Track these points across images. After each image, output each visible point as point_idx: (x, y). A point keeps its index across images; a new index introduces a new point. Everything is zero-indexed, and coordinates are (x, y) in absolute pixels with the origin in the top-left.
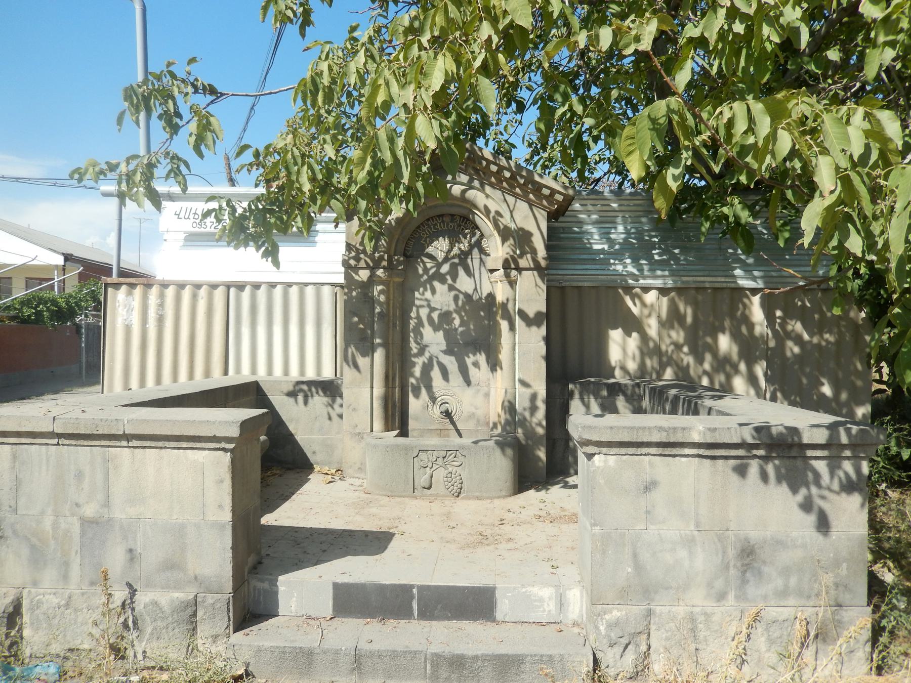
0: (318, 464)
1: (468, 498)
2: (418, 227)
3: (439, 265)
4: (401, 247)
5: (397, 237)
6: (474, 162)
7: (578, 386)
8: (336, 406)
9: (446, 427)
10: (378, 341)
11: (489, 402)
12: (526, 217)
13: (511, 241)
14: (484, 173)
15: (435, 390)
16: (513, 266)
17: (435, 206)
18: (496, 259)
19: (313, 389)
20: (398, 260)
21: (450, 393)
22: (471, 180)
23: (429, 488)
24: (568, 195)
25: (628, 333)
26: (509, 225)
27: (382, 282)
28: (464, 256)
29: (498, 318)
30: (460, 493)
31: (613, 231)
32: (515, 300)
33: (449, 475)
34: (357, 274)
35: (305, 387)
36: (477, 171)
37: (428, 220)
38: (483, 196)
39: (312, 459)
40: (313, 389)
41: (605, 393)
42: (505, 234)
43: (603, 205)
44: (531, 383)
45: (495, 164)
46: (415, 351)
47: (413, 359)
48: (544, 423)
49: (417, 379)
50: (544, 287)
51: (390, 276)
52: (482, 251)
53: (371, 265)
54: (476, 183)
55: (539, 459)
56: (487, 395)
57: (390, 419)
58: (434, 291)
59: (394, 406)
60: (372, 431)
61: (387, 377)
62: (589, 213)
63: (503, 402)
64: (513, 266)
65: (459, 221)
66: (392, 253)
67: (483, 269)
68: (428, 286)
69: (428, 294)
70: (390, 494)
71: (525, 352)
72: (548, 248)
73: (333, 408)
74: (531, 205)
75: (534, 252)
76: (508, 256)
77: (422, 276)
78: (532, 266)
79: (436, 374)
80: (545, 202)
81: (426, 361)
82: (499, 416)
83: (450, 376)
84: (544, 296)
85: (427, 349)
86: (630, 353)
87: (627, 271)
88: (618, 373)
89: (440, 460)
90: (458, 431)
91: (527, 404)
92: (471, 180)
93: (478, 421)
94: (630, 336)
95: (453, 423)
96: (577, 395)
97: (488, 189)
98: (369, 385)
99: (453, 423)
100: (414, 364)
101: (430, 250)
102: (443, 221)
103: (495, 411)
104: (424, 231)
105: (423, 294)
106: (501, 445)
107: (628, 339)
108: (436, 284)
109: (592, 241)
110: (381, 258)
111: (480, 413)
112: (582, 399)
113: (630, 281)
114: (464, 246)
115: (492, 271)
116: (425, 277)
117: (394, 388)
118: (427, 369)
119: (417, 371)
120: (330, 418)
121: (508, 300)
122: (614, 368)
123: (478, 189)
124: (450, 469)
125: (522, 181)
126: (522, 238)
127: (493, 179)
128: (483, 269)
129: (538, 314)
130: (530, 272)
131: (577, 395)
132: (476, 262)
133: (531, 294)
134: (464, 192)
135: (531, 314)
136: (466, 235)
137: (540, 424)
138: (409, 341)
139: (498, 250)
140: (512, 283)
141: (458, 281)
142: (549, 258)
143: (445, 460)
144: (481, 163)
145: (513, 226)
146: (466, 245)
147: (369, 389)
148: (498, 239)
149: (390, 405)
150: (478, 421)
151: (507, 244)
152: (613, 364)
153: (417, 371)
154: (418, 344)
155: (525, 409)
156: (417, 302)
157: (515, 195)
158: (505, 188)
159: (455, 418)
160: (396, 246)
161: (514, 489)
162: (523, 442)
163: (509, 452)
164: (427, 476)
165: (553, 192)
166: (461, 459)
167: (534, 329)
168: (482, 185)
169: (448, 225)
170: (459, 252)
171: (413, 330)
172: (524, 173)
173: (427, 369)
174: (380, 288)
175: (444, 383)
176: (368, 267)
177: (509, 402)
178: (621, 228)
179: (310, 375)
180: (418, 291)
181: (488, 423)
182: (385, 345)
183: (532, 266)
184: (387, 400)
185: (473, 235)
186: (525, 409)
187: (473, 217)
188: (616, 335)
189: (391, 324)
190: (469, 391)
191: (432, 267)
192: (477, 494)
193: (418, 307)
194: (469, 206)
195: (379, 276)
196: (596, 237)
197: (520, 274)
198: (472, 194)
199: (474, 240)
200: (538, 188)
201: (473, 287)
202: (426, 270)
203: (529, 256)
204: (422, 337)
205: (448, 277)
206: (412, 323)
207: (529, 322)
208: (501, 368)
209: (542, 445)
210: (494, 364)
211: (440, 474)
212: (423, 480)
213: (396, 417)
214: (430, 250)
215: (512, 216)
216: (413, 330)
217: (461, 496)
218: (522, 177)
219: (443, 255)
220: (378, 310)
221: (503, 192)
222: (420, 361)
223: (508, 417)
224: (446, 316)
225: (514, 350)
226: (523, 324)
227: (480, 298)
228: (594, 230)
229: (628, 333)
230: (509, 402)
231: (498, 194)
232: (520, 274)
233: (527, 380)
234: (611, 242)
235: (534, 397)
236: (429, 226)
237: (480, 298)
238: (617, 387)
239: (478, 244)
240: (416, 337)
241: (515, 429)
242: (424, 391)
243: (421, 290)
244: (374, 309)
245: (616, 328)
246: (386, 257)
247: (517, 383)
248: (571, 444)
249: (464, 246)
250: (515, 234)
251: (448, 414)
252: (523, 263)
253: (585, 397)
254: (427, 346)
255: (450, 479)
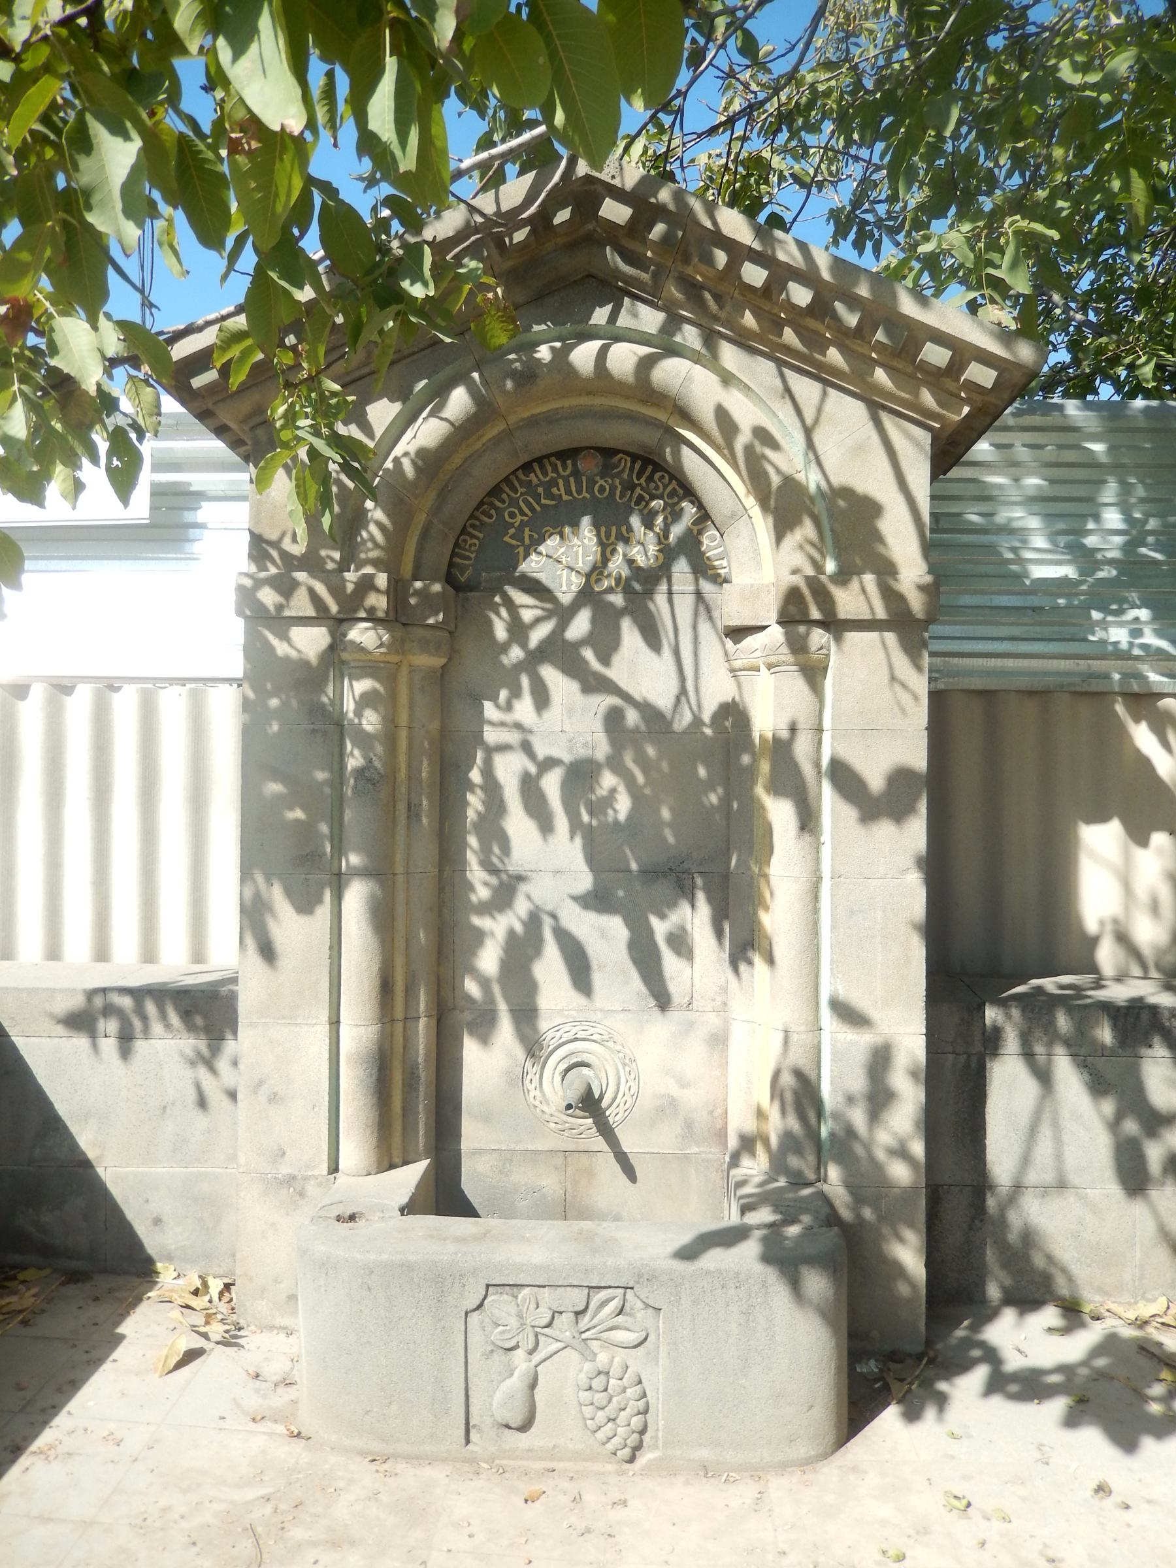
0: (169, 1258)
1: (666, 1469)
2: (495, 491)
3: (565, 615)
4: (439, 554)
5: (421, 518)
6: (686, 260)
7: (1015, 1013)
8: (222, 1064)
9: (583, 1144)
10: (354, 859)
11: (724, 1065)
12: (859, 449)
13: (807, 530)
14: (717, 298)
15: (544, 1025)
16: (815, 614)
17: (551, 419)
18: (754, 593)
19: (151, 1008)
20: (423, 594)
21: (597, 1031)
22: (673, 322)
23: (525, 1427)
24: (1018, 366)
25: (1139, 836)
26: (801, 477)
27: (368, 668)
28: (644, 583)
29: (760, 791)
30: (638, 1447)
31: (1091, 525)
32: (820, 730)
33: (598, 1383)
34: (285, 637)
35: (126, 1002)
36: (693, 290)
37: (527, 467)
38: (712, 379)
39: (151, 1240)
40: (151, 1008)
41: (1105, 1034)
42: (786, 505)
43: (1060, 447)
44: (874, 1014)
45: (758, 258)
46: (483, 893)
47: (476, 921)
48: (918, 1148)
49: (485, 983)
50: (920, 684)
51: (398, 646)
52: (703, 568)
53: (334, 608)
54: (690, 336)
55: (898, 1270)
56: (719, 1041)
57: (398, 1127)
58: (542, 699)
59: (410, 1083)
60: (334, 1169)
61: (386, 987)
62: (1012, 466)
63: (776, 1075)
64: (815, 614)
65: (627, 466)
66: (407, 569)
67: (704, 628)
68: (525, 681)
69: (524, 709)
70: (376, 1446)
71: (851, 905)
72: (928, 548)
73: (212, 1070)
74: (876, 405)
75: (886, 570)
76: (797, 580)
77: (504, 648)
78: (881, 613)
79: (550, 969)
80: (927, 398)
81: (519, 928)
82: (761, 1114)
83: (597, 978)
84: (920, 715)
85: (523, 888)
86: (1141, 891)
87: (1144, 646)
88: (1107, 956)
89: (564, 1326)
90: (622, 1159)
91: (858, 1083)
92: (673, 322)
93: (689, 1126)
94: (1143, 842)
95: (606, 1131)
96: (1011, 1042)
97: (730, 355)
98: (324, 1016)
99: (606, 1131)
100: (479, 937)
101: (532, 565)
102: (576, 473)
103: (748, 1095)
104: (514, 503)
105: (509, 707)
106: (784, 1260)
107: (1140, 854)
108: (550, 674)
109: (1028, 555)
110: (366, 585)
111: (694, 1098)
112: (1028, 1055)
113: (1153, 677)
114: (643, 549)
115: (738, 633)
116: (516, 653)
117: (410, 1019)
118: (521, 952)
119: (489, 960)
120: (202, 1102)
121: (793, 729)
122: (1094, 942)
123: (696, 359)
124: (603, 1358)
125: (852, 320)
126: (847, 525)
127: (749, 319)
128: (704, 628)
129: (900, 777)
130: (873, 636)
131: (1011, 1042)
132: (685, 605)
133: (873, 704)
134: (646, 364)
135: (876, 781)
136: (653, 514)
137: (901, 1152)
138: (464, 862)
139: (758, 562)
140: (813, 673)
141: (616, 659)
142: (931, 591)
143: (585, 1321)
144: (709, 260)
145: (812, 480)
146: (652, 549)
147: (324, 1030)
148: (762, 524)
149: (397, 1078)
150: (689, 1126)
151: (793, 539)
152: (1091, 925)
153: (489, 960)
154: (493, 870)
155: (850, 1100)
156: (491, 736)
157: (824, 376)
158: (788, 349)
159: (614, 1115)
160: (420, 549)
161: (838, 1427)
162: (846, 1214)
163: (816, 1283)
164: (516, 1383)
165: (963, 353)
166: (643, 1317)
167: (885, 829)
168: (710, 339)
169: (592, 483)
170: (625, 572)
171: (479, 827)
172: (863, 291)
173: (521, 952)
174: (363, 686)
175: (577, 999)
176: (321, 616)
177: (799, 1074)
178: (1113, 518)
179: (127, 967)
180: (494, 699)
181: (722, 1134)
182: (380, 871)
183: (881, 613)
184: (386, 1069)
185: (675, 515)
186: (850, 1100)
187: (677, 454)
188: (1100, 843)
189: (402, 807)
190: (660, 1028)
191: (537, 621)
192: (704, 1454)
193: (490, 751)
194: (662, 416)
195: (359, 648)
196: (1040, 542)
197: (838, 639)
198: (672, 372)
199: (676, 531)
200: (911, 337)
201: (673, 687)
202: (519, 631)
203: (869, 579)
204: (506, 849)
205: (588, 654)
206: (475, 802)
207: (876, 805)
208: (770, 960)
209: (911, 1225)
210: (745, 944)
211: (564, 1376)
212: (498, 1397)
213: (416, 1111)
214: (532, 565)
215: (810, 445)
216: (479, 827)
217: (644, 1458)
218: (853, 302)
219: (577, 582)
220: (354, 760)
221: (780, 364)
222: (497, 928)
223: (794, 1124)
224: (580, 775)
225: (816, 898)
226: (850, 813)
227: (697, 721)
228: (1034, 523)
229: (1139, 836)
230: (799, 1074)
231: (761, 372)
232: (838, 639)
233: (860, 1001)
234: (1087, 559)
235: (880, 1061)
236: (530, 488)
237: (697, 721)
238: (1145, 1016)
239: (691, 546)
240: (486, 850)
241: (820, 1166)
242: (505, 1028)
243: (503, 694)
244: (341, 756)
245: (1099, 816)
246: (382, 580)
247: (826, 1012)
248: (991, 1203)
249: (643, 549)
250: (820, 508)
251: (590, 1104)
252: (851, 601)
253: (1039, 1049)
254: (520, 878)
255: (600, 1398)
